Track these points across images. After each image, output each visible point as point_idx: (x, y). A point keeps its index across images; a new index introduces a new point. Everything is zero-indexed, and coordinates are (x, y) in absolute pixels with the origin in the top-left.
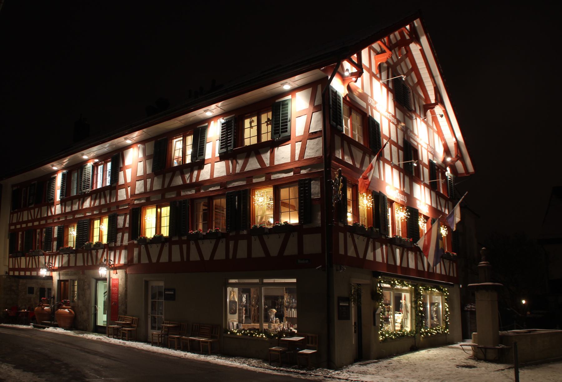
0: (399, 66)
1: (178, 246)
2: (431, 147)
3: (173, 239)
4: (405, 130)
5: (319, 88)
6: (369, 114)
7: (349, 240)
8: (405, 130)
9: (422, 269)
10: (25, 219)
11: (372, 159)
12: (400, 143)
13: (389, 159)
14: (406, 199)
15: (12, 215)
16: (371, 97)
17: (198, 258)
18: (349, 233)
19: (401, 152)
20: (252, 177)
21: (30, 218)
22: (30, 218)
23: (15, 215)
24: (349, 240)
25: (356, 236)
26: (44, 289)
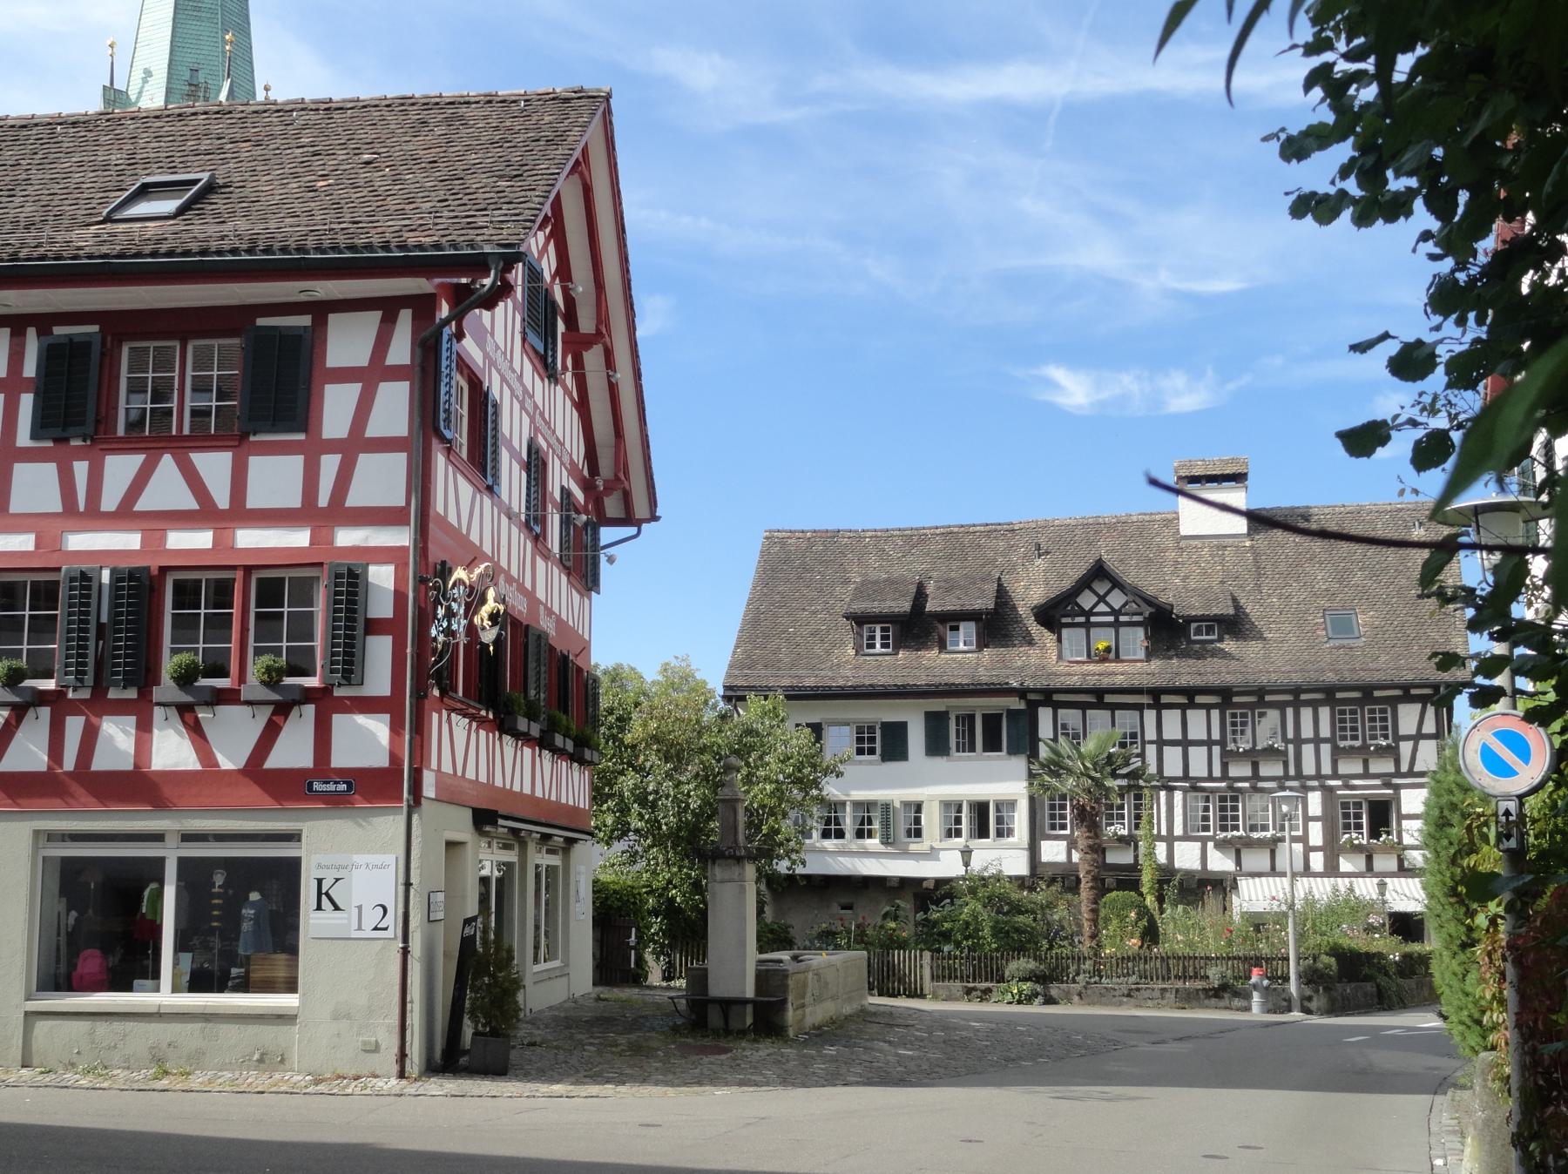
5: (405, 317)
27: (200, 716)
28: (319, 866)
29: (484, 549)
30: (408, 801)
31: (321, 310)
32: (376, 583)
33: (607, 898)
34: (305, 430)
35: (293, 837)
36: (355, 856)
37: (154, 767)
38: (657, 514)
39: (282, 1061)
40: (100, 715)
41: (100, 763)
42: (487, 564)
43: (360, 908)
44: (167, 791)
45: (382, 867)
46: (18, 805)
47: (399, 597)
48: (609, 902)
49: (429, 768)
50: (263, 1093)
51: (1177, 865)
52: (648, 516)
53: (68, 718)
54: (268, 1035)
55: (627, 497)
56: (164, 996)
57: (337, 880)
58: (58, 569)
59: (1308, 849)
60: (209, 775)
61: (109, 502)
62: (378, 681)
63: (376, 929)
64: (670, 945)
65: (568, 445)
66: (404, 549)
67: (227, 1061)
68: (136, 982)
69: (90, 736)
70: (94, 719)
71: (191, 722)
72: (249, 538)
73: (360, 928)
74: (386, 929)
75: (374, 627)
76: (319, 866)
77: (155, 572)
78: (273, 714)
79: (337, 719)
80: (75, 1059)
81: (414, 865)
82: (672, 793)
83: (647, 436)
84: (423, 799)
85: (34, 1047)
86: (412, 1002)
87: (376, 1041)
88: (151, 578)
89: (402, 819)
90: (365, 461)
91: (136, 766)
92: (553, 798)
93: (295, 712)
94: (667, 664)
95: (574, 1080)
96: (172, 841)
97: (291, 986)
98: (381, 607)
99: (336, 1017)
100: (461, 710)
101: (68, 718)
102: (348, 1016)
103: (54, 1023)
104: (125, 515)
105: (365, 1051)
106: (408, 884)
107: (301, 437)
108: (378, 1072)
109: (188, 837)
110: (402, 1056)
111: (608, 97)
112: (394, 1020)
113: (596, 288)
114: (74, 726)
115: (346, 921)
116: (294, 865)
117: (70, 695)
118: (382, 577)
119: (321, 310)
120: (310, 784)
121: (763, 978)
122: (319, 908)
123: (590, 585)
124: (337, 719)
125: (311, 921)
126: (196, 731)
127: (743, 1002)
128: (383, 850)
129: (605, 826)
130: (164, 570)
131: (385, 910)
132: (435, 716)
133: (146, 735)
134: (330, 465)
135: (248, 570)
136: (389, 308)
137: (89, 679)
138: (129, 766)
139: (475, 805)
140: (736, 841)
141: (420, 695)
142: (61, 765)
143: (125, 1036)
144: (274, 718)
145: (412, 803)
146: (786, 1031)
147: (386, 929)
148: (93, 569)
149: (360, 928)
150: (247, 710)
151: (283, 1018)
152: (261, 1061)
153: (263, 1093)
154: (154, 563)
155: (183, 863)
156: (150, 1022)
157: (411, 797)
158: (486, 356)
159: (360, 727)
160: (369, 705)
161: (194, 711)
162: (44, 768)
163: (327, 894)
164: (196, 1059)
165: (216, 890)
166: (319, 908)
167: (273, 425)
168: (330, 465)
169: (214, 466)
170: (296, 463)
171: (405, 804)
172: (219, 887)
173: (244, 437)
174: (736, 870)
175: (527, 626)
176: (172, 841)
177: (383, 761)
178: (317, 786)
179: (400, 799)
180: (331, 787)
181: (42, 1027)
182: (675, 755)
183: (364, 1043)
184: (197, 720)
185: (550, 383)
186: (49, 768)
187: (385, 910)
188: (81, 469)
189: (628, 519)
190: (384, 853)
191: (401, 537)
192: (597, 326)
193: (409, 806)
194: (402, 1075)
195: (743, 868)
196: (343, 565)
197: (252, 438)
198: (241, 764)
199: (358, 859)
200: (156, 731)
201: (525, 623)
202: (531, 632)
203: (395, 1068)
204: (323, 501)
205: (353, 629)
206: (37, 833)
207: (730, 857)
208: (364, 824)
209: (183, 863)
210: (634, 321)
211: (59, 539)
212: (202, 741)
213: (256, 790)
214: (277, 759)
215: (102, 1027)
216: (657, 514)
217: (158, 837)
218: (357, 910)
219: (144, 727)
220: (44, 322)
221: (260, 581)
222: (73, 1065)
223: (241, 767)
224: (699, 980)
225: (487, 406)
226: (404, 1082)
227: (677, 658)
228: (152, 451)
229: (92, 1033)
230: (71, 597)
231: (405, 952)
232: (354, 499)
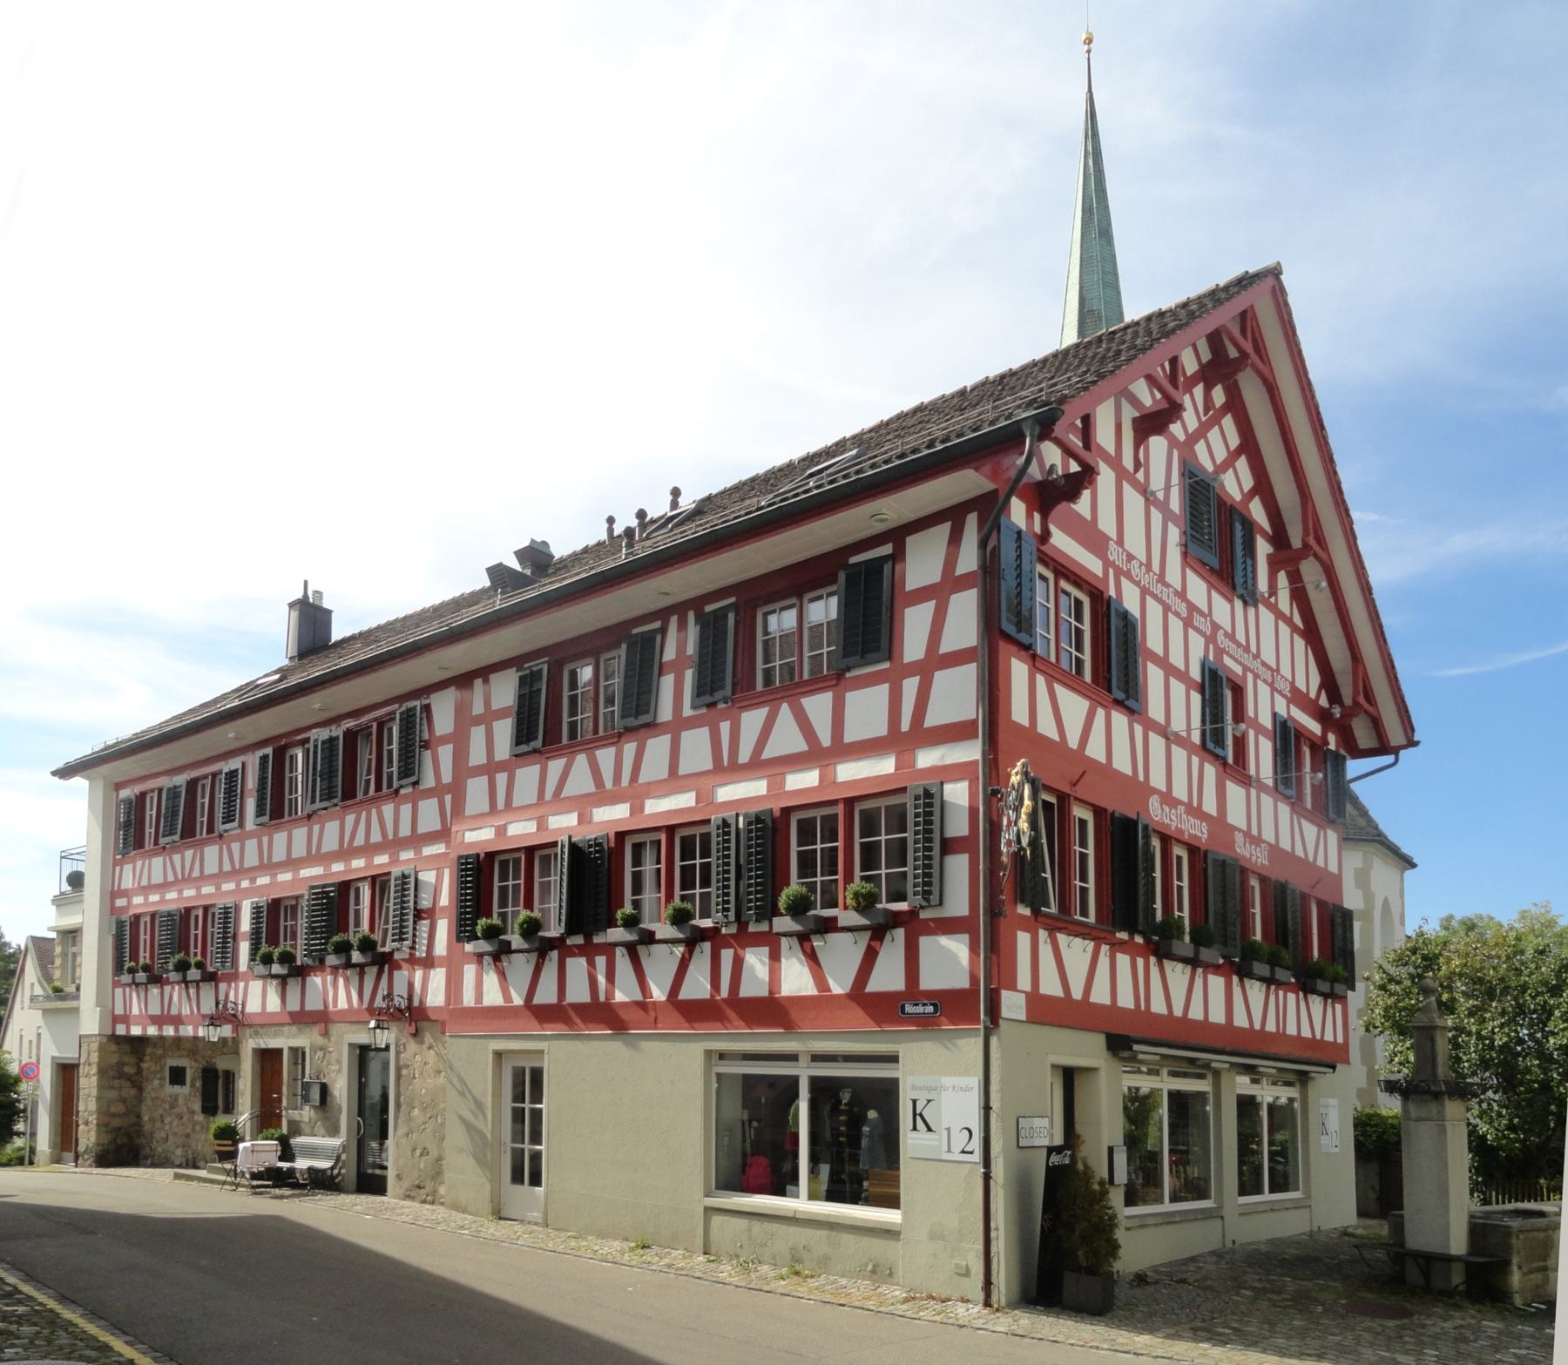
0: (1190, 431)
1: (582, 961)
2: (1283, 677)
3: (569, 942)
4: (1208, 633)
5: (972, 520)
6: (1108, 591)
7: (1046, 951)
8: (1208, 633)
9: (1246, 1025)
10: (157, 878)
11: (1259, 1130)
12: (1195, 674)
13: (1161, 720)
14: (1204, 831)
15: (118, 868)
16: (1116, 543)
17: (1107, 1001)
18: (1046, 933)
19: (1196, 698)
20: (784, 773)
21: (171, 878)
22: (171, 878)
23: (128, 868)
24: (1046, 951)
25: (1062, 938)
26: (215, 1071)
27: (815, 944)
28: (914, 1087)
29: (1116, 765)
30: (984, 1022)
31: (898, 535)
32: (953, 801)
33: (1384, 1132)
34: (890, 658)
35: (893, 1059)
36: (943, 1078)
37: (783, 994)
38: (1416, 739)
39: (891, 1275)
40: (743, 948)
41: (746, 991)
42: (1023, 760)
43: (948, 1130)
44: (795, 1015)
45: (967, 1090)
46: (693, 1028)
47: (973, 811)
48: (1385, 1137)
49: (1013, 987)
50: (843, 1305)
51: (96, 1032)
52: (1403, 741)
53: (723, 951)
54: (877, 1246)
55: (1376, 724)
56: (799, 1203)
57: (929, 1101)
58: (708, 821)
59: (459, 740)
60: (822, 1002)
61: (744, 756)
62: (958, 902)
63: (963, 1152)
64: (1484, 1183)
65: (1286, 670)
66: (976, 762)
67: (848, 1268)
68: (788, 1187)
69: (738, 963)
70: (740, 951)
71: (809, 951)
72: (851, 772)
73: (949, 1151)
74: (971, 1153)
75: (949, 846)
76: (914, 1087)
77: (777, 813)
78: (872, 939)
79: (924, 942)
80: (739, 1251)
81: (994, 1087)
82: (1474, 1030)
83: (1389, 655)
84: (1000, 1020)
85: (712, 1238)
86: (997, 1229)
87: (967, 1266)
88: (774, 820)
89: (980, 1040)
90: (940, 677)
91: (771, 992)
92: (1271, 1027)
93: (888, 937)
94: (1525, 911)
95: (1173, 1331)
96: (804, 1060)
97: (892, 1202)
98: (958, 826)
99: (933, 1237)
100: (1089, 934)
101: (723, 951)
102: (942, 1238)
103: (727, 1218)
104: (757, 765)
105: (957, 1274)
106: (987, 1109)
107: (886, 665)
108: (970, 1297)
109: (817, 1058)
110: (988, 1283)
111: (1275, 272)
112: (980, 1246)
113: (1301, 498)
114: (727, 955)
115: (936, 1143)
116: (894, 1083)
117: (724, 931)
118: (957, 794)
119: (898, 535)
120: (903, 1007)
121: (1479, 1231)
122: (915, 1128)
123: (1332, 815)
124: (924, 942)
125: (909, 1141)
126: (812, 957)
127: (1448, 1259)
128: (967, 1073)
129: (1408, 1062)
130: (787, 811)
131: (970, 1133)
132: (1023, 939)
133: (777, 964)
134: (911, 686)
135: (850, 802)
136: (954, 515)
137: (732, 915)
138: (765, 993)
139: (1108, 1031)
140: (1434, 1073)
141: (994, 912)
142: (719, 994)
143: (772, 1235)
144: (873, 943)
145: (989, 1024)
146: (1510, 1298)
147: (971, 1153)
148: (731, 816)
149: (949, 1151)
150: (848, 936)
151: (888, 1233)
152: (874, 1271)
153: (843, 1305)
154: (776, 806)
155: (815, 1082)
156: (790, 1225)
157: (988, 1019)
158: (1107, 564)
159: (943, 948)
160: (948, 926)
161: (810, 940)
162: (708, 996)
163: (921, 1115)
164: (824, 1264)
165: (843, 1107)
166: (915, 1128)
167: (862, 657)
168: (911, 686)
169: (818, 706)
170: (882, 692)
171: (981, 1027)
172: (846, 1104)
173: (840, 676)
174: (1433, 1108)
175: (1206, 852)
176: (804, 1060)
177: (963, 983)
178: (909, 1009)
179: (977, 1021)
180: (920, 1009)
181: (717, 1220)
182: (1487, 991)
183: (957, 1266)
184: (813, 949)
185: (1245, 603)
186: (712, 996)
187: (970, 1133)
188: (725, 727)
189: (1383, 748)
190: (969, 1076)
191: (970, 752)
192: (1303, 540)
193: (986, 1028)
194: (987, 1304)
195: (1443, 1106)
196: (918, 786)
197: (848, 675)
198: (848, 990)
199: (947, 1081)
200: (783, 960)
201: (1203, 848)
202: (1210, 856)
203: (981, 1296)
204: (905, 726)
205: (930, 849)
206: (708, 1053)
207: (1425, 1093)
208: (949, 1045)
209: (815, 1082)
210: (1352, 529)
211: (713, 794)
212: (816, 966)
213: (860, 1013)
214: (875, 985)
215: (758, 1227)
216: (1416, 739)
217: (792, 1057)
218: (946, 1132)
219: (775, 957)
220: (697, 603)
221: (862, 812)
222: (737, 1256)
223: (848, 991)
224: (1398, 1229)
225: (1109, 616)
226: (986, 1311)
227: (1535, 905)
228: (775, 702)
229: (749, 1230)
230: (750, 847)
231: (987, 1177)
232: (932, 719)
